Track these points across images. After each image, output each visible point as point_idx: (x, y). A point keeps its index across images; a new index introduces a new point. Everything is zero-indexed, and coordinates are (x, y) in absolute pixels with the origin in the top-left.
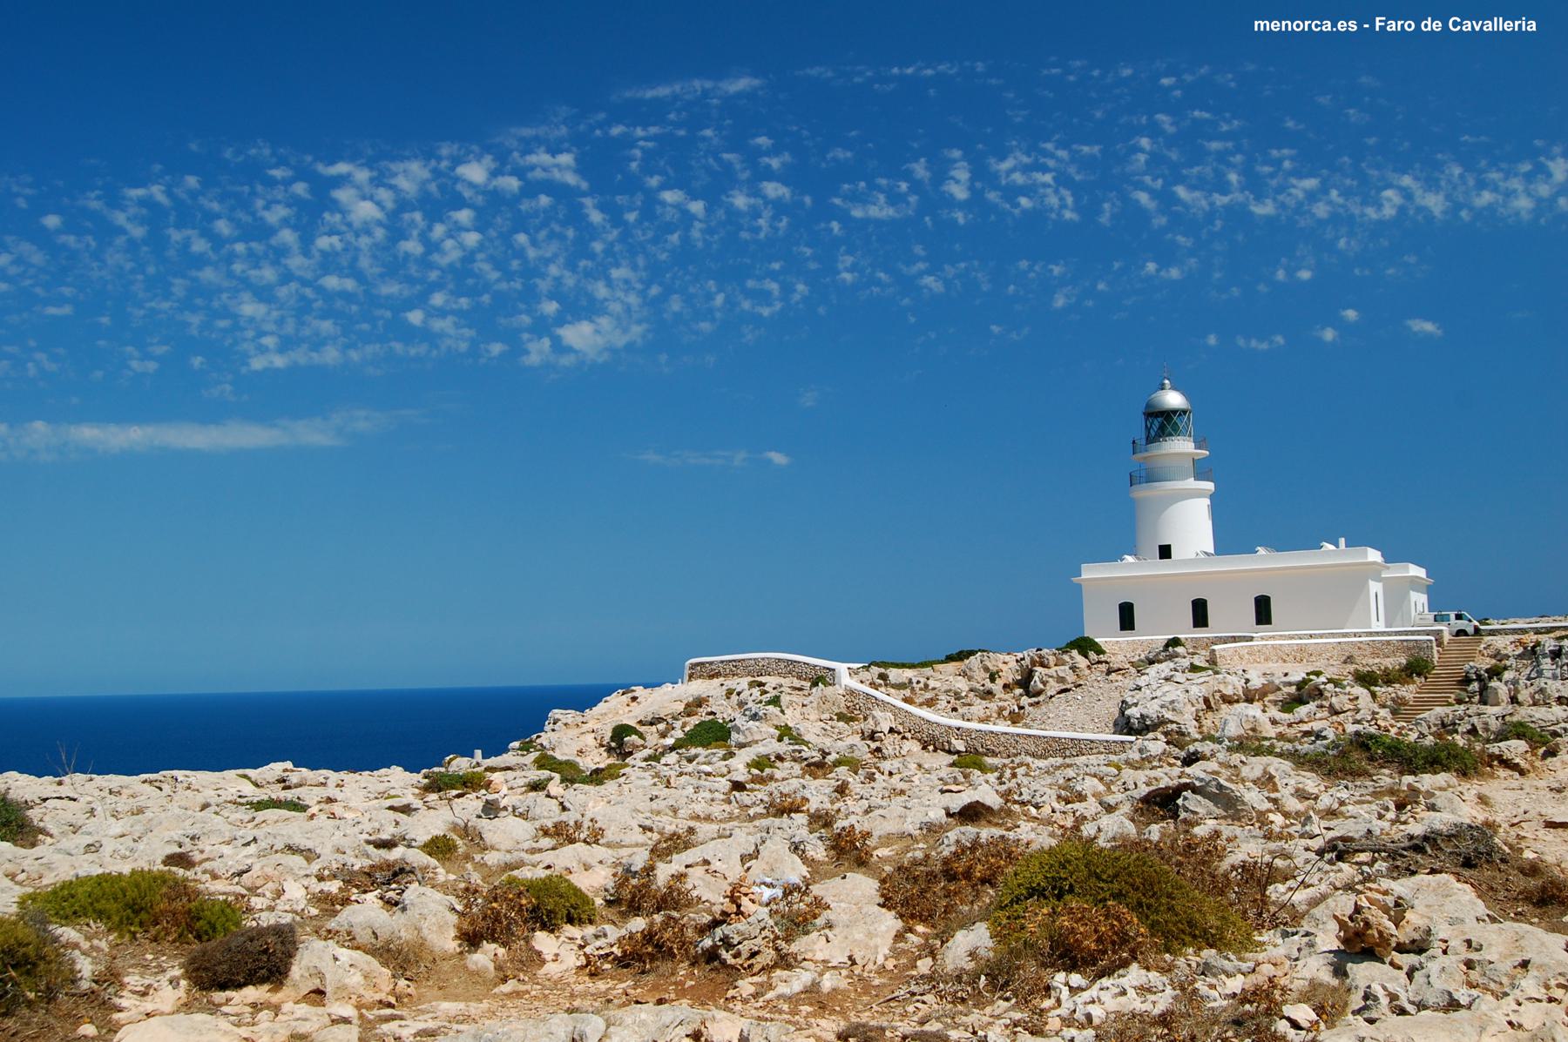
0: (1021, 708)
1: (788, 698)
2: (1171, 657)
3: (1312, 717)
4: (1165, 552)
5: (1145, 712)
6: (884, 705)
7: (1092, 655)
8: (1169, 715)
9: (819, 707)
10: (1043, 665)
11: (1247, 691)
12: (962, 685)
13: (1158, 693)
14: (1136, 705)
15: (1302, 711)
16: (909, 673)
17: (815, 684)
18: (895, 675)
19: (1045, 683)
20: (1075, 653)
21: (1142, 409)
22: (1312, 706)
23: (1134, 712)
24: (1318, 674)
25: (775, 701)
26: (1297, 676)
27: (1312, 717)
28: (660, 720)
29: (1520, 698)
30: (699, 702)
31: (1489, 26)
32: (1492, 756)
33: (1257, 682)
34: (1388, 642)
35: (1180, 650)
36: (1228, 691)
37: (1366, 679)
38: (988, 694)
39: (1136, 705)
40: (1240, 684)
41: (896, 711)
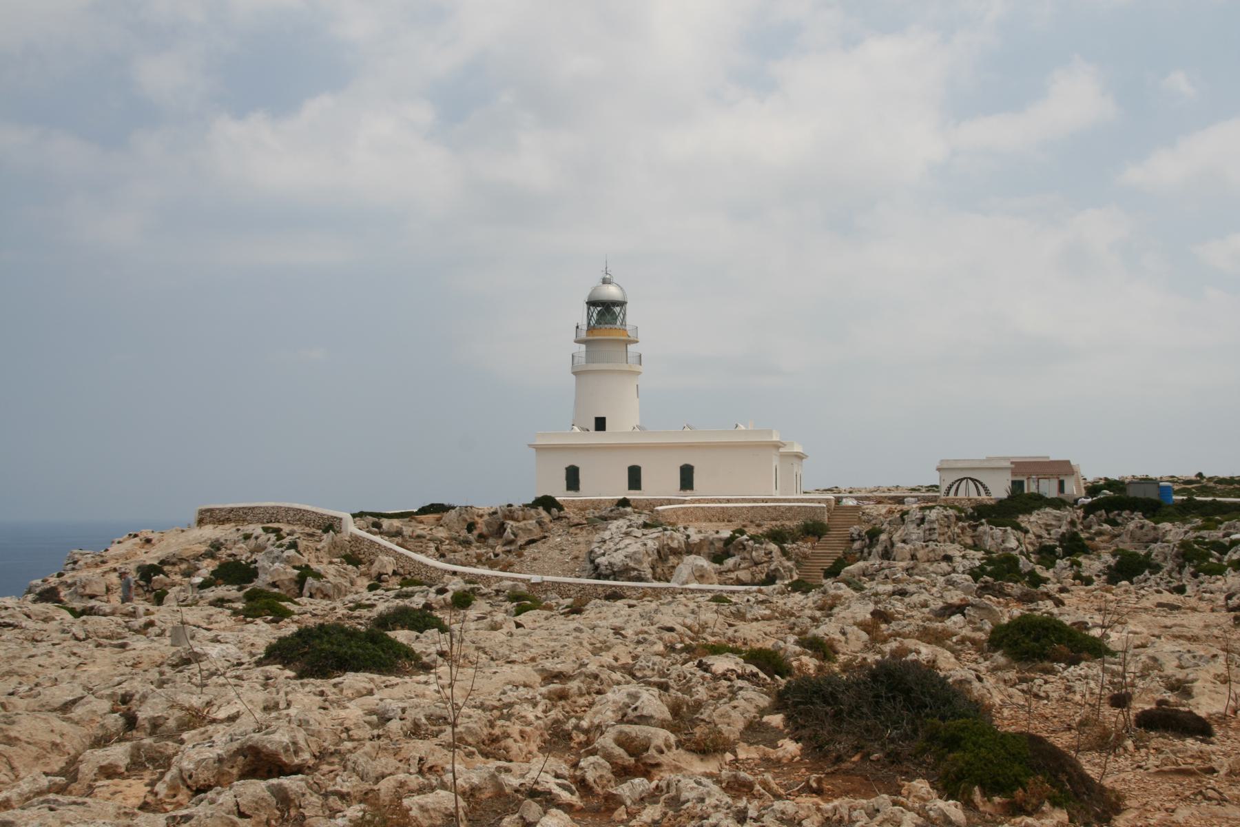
0: (496, 555)
1: (305, 543)
2: (623, 515)
3: (736, 567)
4: (600, 424)
5: (612, 560)
6: (387, 551)
7: (554, 511)
8: (632, 564)
9: (330, 551)
10: (513, 519)
11: (687, 544)
12: (441, 533)
13: (622, 545)
14: (604, 554)
15: (730, 562)
16: (396, 523)
17: (326, 531)
18: (386, 523)
19: (516, 536)
20: (541, 508)
21: (585, 297)
22: (736, 559)
23: (602, 560)
24: (742, 532)
25: (293, 545)
26: (726, 534)
27: (736, 567)
28: (182, 560)
29: (919, 556)
30: (216, 546)
31: (1210, 499)
32: (1043, 593)
33: (695, 538)
34: (791, 508)
35: (629, 509)
36: (675, 545)
37: (777, 536)
38: (466, 543)
39: (604, 554)
40: (682, 539)
41: (398, 556)
